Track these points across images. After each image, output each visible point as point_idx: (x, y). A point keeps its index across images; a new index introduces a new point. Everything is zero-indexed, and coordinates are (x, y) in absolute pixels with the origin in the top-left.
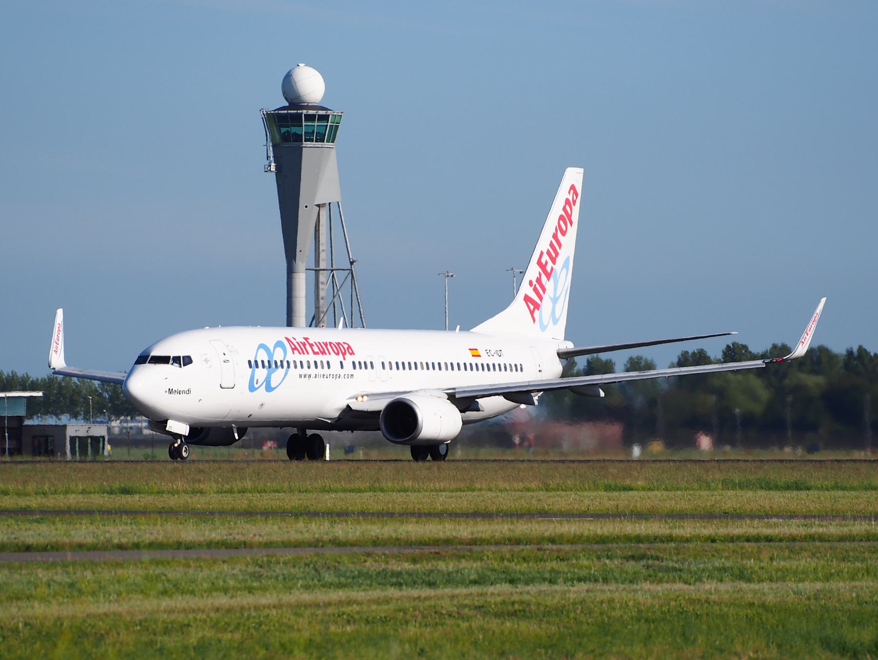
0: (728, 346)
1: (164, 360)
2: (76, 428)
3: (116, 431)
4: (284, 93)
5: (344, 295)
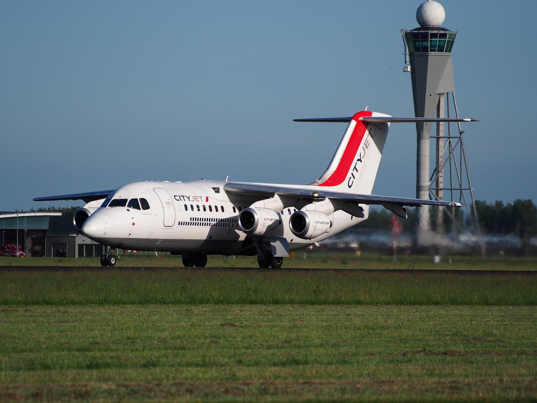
1: (121, 203)
4: (418, 19)
5: (457, 152)
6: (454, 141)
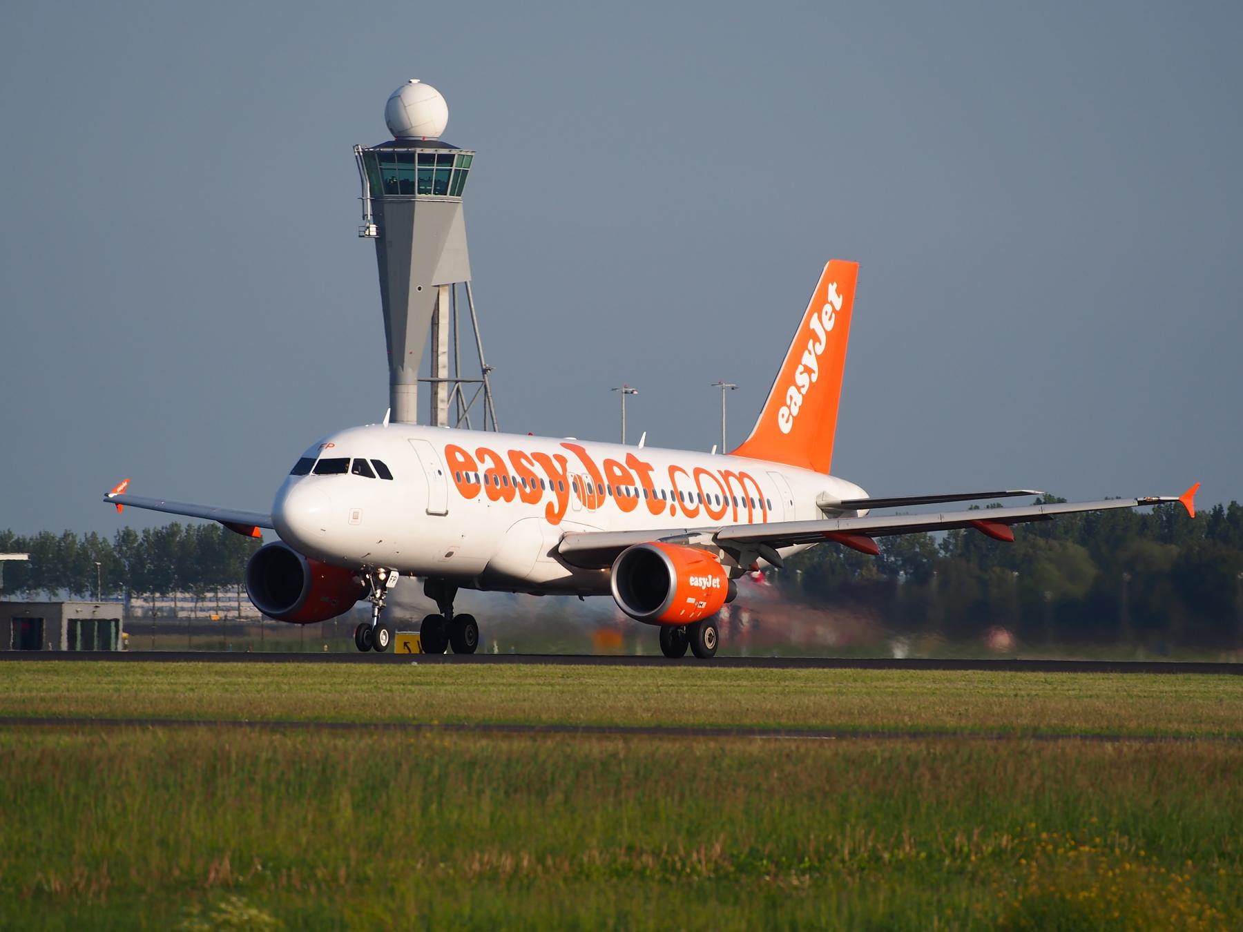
2: (76, 608)
3: (139, 613)
4: (389, 123)
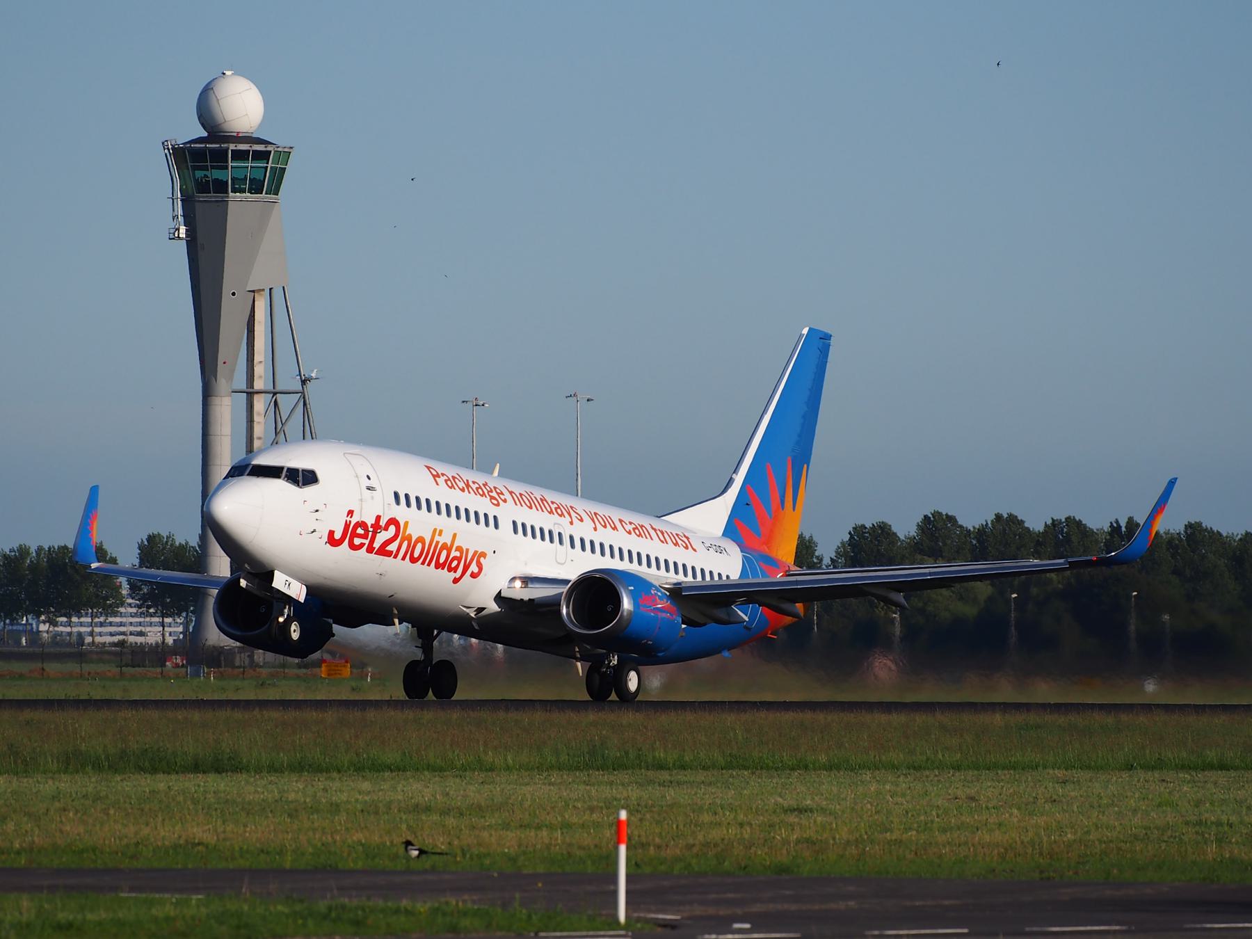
0: (926, 516)
6: (286, 402)
